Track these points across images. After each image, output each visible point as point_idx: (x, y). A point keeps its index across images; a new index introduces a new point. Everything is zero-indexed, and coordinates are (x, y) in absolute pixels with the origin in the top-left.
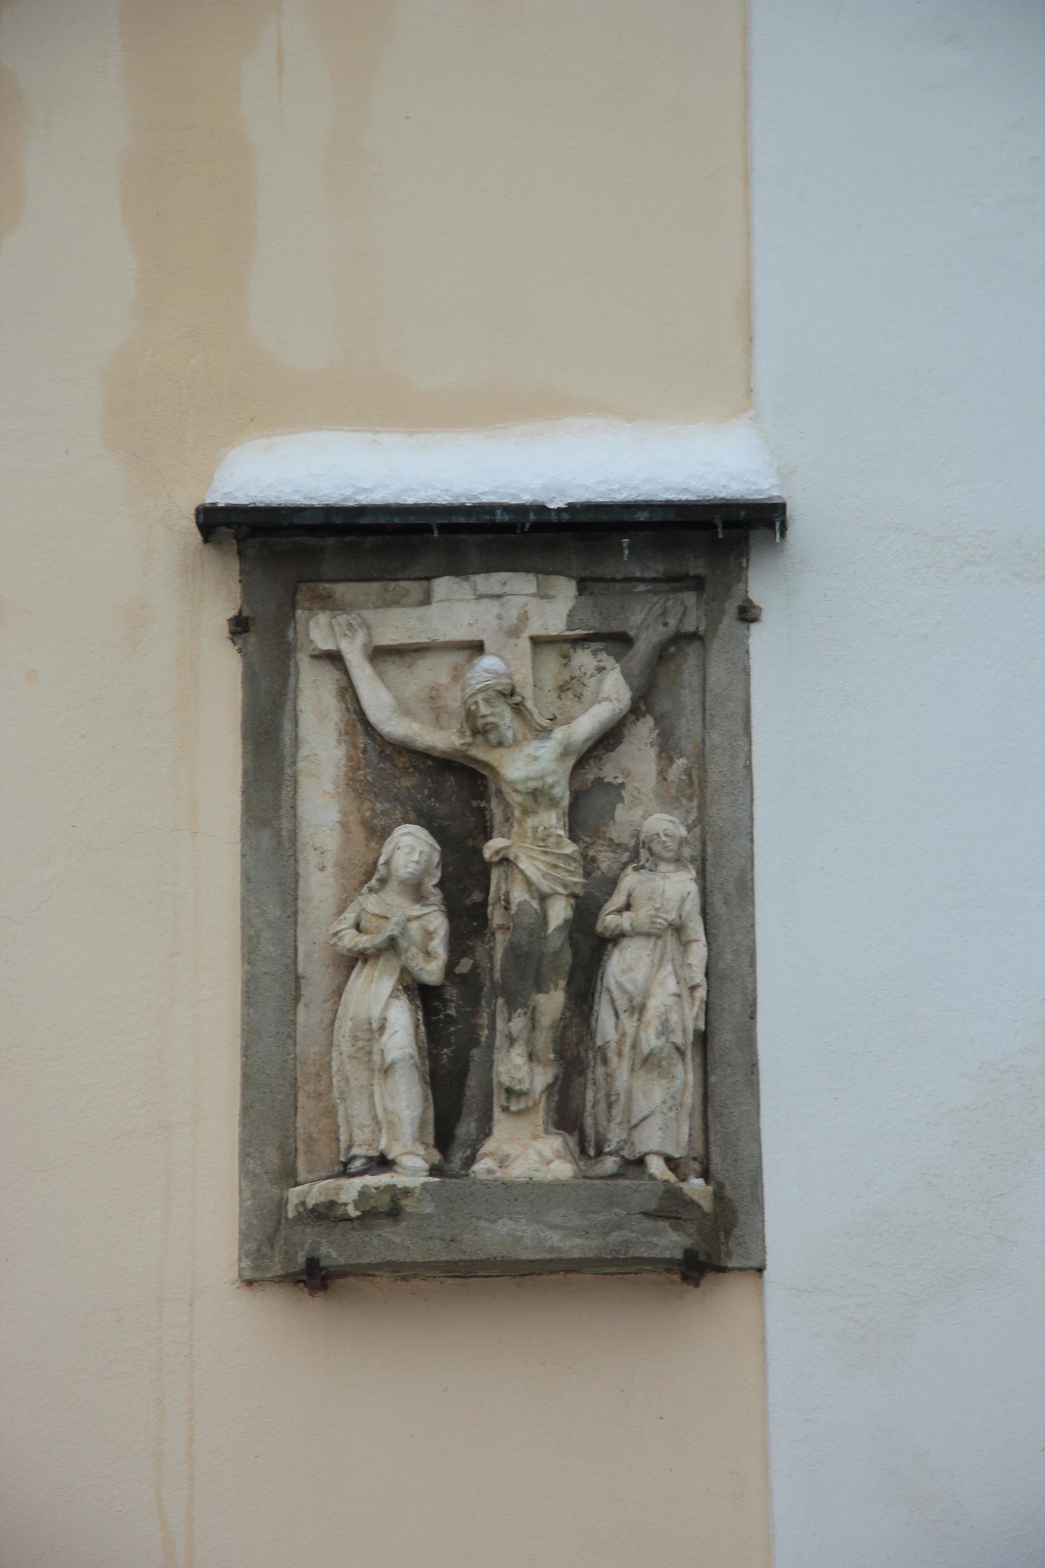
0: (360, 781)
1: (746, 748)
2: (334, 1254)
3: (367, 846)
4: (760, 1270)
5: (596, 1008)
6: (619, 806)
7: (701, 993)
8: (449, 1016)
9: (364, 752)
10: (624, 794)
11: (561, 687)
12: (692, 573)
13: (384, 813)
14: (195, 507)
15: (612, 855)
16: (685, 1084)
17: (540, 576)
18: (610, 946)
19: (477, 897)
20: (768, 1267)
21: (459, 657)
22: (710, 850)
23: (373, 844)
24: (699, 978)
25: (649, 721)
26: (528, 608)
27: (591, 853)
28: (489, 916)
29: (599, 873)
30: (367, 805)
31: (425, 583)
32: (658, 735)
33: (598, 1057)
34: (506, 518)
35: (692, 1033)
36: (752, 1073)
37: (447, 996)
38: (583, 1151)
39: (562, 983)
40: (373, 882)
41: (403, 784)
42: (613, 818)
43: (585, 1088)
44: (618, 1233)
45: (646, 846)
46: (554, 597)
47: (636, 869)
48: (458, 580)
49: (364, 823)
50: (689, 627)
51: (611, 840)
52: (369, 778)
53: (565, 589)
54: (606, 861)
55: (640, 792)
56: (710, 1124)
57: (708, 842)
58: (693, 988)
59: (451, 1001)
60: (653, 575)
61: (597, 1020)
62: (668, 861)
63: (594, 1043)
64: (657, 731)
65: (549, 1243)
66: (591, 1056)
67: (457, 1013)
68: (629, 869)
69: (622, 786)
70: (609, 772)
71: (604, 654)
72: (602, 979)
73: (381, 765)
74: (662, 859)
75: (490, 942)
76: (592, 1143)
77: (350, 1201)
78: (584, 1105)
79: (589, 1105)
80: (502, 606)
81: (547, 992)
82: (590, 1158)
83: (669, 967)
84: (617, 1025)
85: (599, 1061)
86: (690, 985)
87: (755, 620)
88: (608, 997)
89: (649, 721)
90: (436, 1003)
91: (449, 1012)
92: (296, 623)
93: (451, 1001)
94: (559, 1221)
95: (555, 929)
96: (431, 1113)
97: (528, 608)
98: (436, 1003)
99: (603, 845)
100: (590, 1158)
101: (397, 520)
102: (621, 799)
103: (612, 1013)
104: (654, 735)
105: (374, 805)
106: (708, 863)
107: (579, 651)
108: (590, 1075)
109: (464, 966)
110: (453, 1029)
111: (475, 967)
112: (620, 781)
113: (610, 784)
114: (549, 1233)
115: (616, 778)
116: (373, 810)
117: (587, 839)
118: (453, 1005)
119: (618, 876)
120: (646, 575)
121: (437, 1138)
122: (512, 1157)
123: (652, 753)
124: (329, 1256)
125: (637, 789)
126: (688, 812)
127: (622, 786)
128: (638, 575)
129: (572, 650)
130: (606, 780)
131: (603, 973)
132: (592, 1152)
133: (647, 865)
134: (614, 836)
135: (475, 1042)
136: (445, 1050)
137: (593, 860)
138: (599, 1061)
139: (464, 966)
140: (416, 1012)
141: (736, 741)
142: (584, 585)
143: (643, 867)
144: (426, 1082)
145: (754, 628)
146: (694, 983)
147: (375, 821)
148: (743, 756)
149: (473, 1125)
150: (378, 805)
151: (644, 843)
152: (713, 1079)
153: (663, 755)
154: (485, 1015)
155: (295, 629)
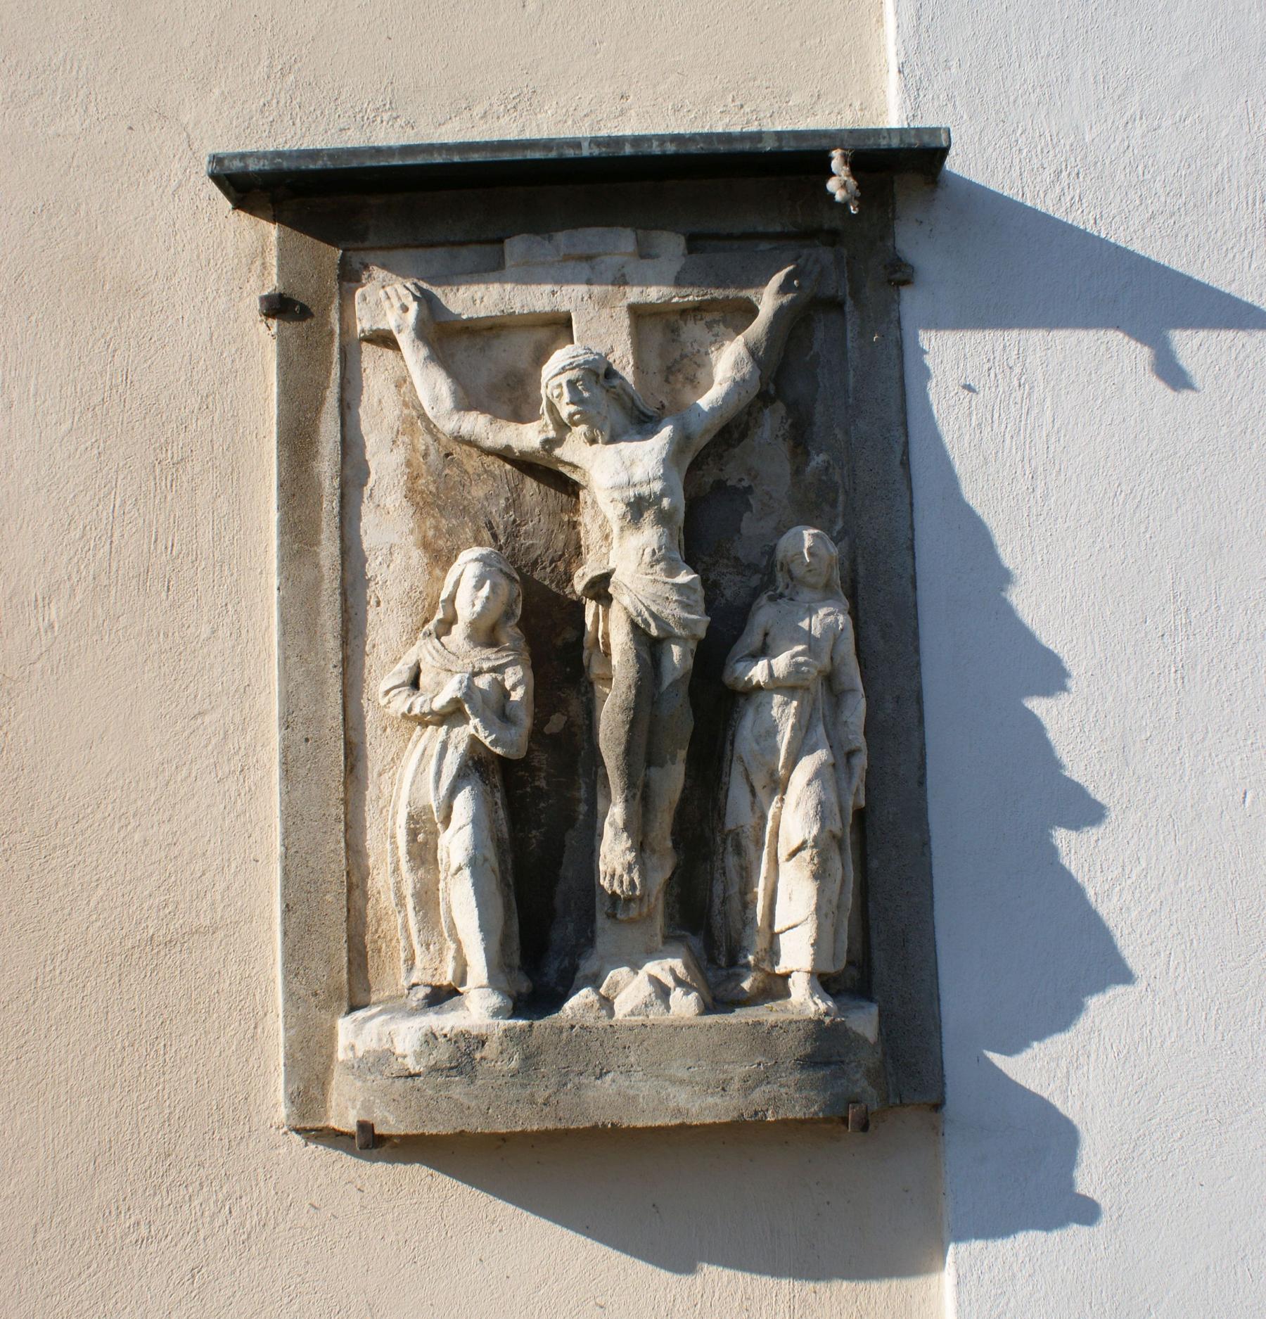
0: (422, 492)
1: (903, 439)
2: (392, 1119)
3: (430, 573)
4: (938, 1106)
5: (725, 779)
6: (747, 515)
7: (861, 762)
8: (538, 788)
9: (425, 456)
10: (752, 501)
11: (669, 368)
12: (826, 227)
13: (450, 532)
14: (1081, 1128)
15: (738, 578)
16: (843, 881)
17: (639, 231)
18: (742, 701)
19: (569, 635)
20: (948, 1102)
21: (542, 334)
22: (861, 570)
23: (437, 572)
24: (860, 741)
25: (780, 408)
26: (625, 270)
27: (712, 577)
28: (585, 662)
29: (723, 601)
30: (430, 522)
31: (497, 247)
32: (792, 426)
33: (729, 842)
34: (596, 152)
35: (851, 812)
36: (923, 854)
37: (535, 763)
38: (712, 960)
39: (682, 754)
40: (431, 626)
41: (474, 493)
42: (739, 531)
43: (712, 879)
44: (767, 1088)
45: (785, 569)
46: (657, 256)
47: (772, 599)
48: (538, 238)
49: (425, 545)
50: (829, 291)
51: (736, 559)
52: (432, 488)
53: (672, 245)
54: (732, 587)
55: (771, 498)
56: (871, 922)
57: (859, 559)
58: (850, 754)
59: (540, 769)
60: (778, 229)
61: (726, 797)
62: (813, 587)
63: (723, 824)
64: (790, 421)
65: (672, 1105)
66: (718, 839)
67: (548, 784)
68: (764, 599)
69: (749, 490)
70: (733, 475)
71: (721, 326)
72: (732, 743)
73: (447, 471)
74: (803, 582)
75: (587, 692)
76: (724, 949)
77: (409, 1051)
78: (711, 901)
79: (717, 902)
80: (593, 268)
81: (662, 766)
82: (720, 967)
83: (821, 730)
84: (753, 803)
85: (730, 849)
86: (847, 749)
87: (906, 282)
88: (742, 769)
89: (780, 408)
90: (520, 773)
91: (537, 783)
92: (784, 792)
93: (540, 769)
94: (683, 1074)
95: (671, 684)
96: (515, 927)
97: (625, 270)
98: (520, 773)
99: (727, 566)
100: (720, 967)
101: (457, 159)
102: (748, 507)
103: (747, 789)
104: (787, 427)
105: (438, 522)
106: (860, 586)
107: (691, 324)
108: (718, 864)
109: (556, 723)
110: (542, 805)
111: (569, 725)
112: (745, 484)
113: (734, 488)
114: (672, 1090)
115: (741, 480)
116: (437, 528)
117: (706, 559)
118: (543, 775)
119: (750, 605)
120: (771, 230)
121: (524, 957)
122: (621, 984)
123: (784, 448)
124: (385, 1122)
125: (767, 493)
126: (833, 521)
127: (749, 490)
128: (760, 229)
129: (681, 323)
130: (729, 483)
131: (734, 736)
132: (723, 961)
133: (787, 592)
134: (740, 554)
135: (570, 821)
136: (534, 832)
137: (716, 585)
138: (730, 849)
139: (556, 723)
140: (492, 793)
141: (889, 431)
142: (695, 243)
143: (781, 596)
144: (508, 885)
145: (906, 293)
146: (853, 747)
147: (441, 542)
148: (898, 449)
149: (571, 927)
150: (444, 521)
151: (782, 564)
152: (874, 864)
153: (799, 451)
154: (583, 786)
155: (782, 800)
